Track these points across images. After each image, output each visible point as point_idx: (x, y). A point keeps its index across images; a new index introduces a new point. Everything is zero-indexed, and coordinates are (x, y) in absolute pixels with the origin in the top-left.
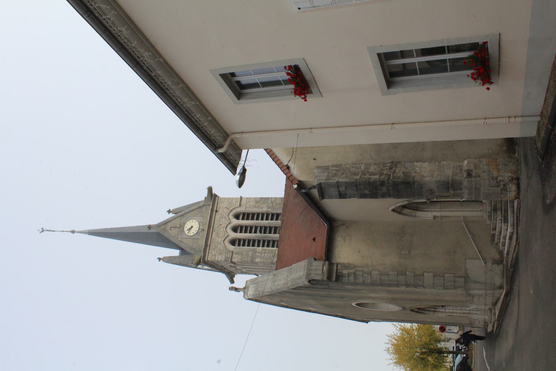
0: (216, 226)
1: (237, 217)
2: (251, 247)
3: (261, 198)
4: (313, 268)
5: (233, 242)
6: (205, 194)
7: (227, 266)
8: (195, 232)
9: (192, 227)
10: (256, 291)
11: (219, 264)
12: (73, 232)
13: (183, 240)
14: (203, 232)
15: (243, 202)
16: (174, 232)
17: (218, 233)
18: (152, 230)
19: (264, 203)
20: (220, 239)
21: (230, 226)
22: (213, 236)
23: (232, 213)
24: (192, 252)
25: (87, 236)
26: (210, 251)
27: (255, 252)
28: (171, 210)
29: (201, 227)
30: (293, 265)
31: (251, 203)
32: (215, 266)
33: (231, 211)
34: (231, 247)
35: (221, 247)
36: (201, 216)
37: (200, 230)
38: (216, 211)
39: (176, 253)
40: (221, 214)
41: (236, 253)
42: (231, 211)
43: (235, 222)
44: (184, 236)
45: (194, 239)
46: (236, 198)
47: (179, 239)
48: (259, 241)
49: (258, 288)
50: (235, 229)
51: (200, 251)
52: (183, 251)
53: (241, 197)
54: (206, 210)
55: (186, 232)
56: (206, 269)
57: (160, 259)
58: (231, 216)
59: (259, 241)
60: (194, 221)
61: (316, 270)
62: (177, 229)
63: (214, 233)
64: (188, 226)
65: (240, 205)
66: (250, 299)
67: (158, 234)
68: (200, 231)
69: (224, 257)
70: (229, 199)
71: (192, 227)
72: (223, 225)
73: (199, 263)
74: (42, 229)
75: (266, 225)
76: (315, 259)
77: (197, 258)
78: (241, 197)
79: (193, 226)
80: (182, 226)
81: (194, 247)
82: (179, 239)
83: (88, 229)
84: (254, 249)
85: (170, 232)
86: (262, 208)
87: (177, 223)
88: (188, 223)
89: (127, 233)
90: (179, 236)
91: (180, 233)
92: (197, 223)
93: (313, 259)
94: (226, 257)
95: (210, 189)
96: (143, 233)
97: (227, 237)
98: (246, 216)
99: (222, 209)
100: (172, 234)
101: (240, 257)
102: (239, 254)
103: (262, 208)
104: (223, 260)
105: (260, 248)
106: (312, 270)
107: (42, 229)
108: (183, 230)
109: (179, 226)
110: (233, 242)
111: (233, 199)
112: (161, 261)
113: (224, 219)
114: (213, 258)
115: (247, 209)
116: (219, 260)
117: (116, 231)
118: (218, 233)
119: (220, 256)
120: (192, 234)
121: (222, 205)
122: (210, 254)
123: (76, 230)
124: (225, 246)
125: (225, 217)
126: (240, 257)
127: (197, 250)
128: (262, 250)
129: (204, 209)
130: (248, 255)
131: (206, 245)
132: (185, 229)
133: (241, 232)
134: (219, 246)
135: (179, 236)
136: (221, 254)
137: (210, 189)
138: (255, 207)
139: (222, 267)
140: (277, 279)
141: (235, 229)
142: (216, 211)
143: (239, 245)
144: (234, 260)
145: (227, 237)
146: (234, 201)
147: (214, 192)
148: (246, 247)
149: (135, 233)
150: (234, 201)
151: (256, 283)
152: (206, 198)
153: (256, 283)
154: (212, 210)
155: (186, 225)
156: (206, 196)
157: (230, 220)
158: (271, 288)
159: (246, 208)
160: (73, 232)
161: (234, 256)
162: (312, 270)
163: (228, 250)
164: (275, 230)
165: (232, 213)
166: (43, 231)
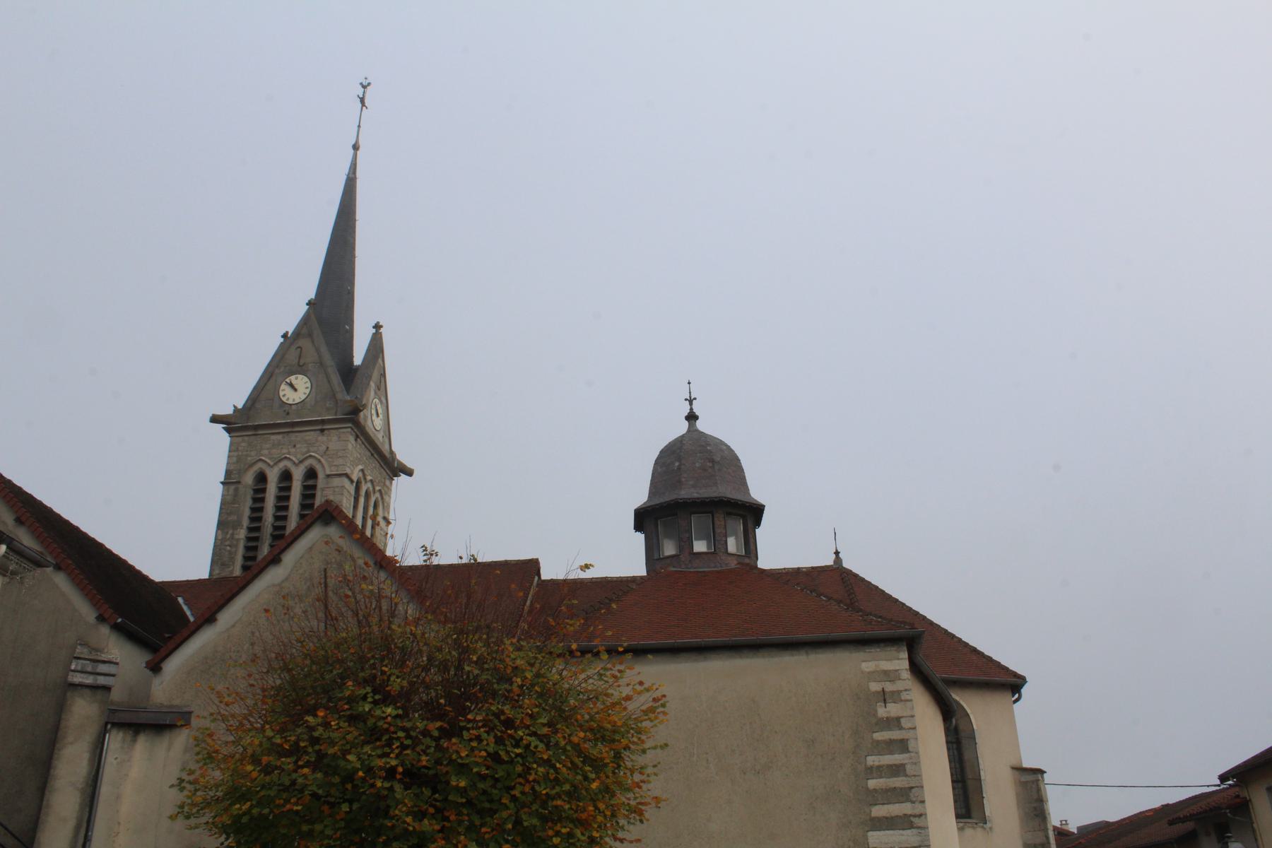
0: (293, 437)
1: (311, 474)
38: (322, 431)
65: (328, 476)
110: (262, 478)
121: (335, 438)
141: (286, 476)
142: (322, 431)
157: (301, 462)
160: (356, 147)
164: (879, 771)
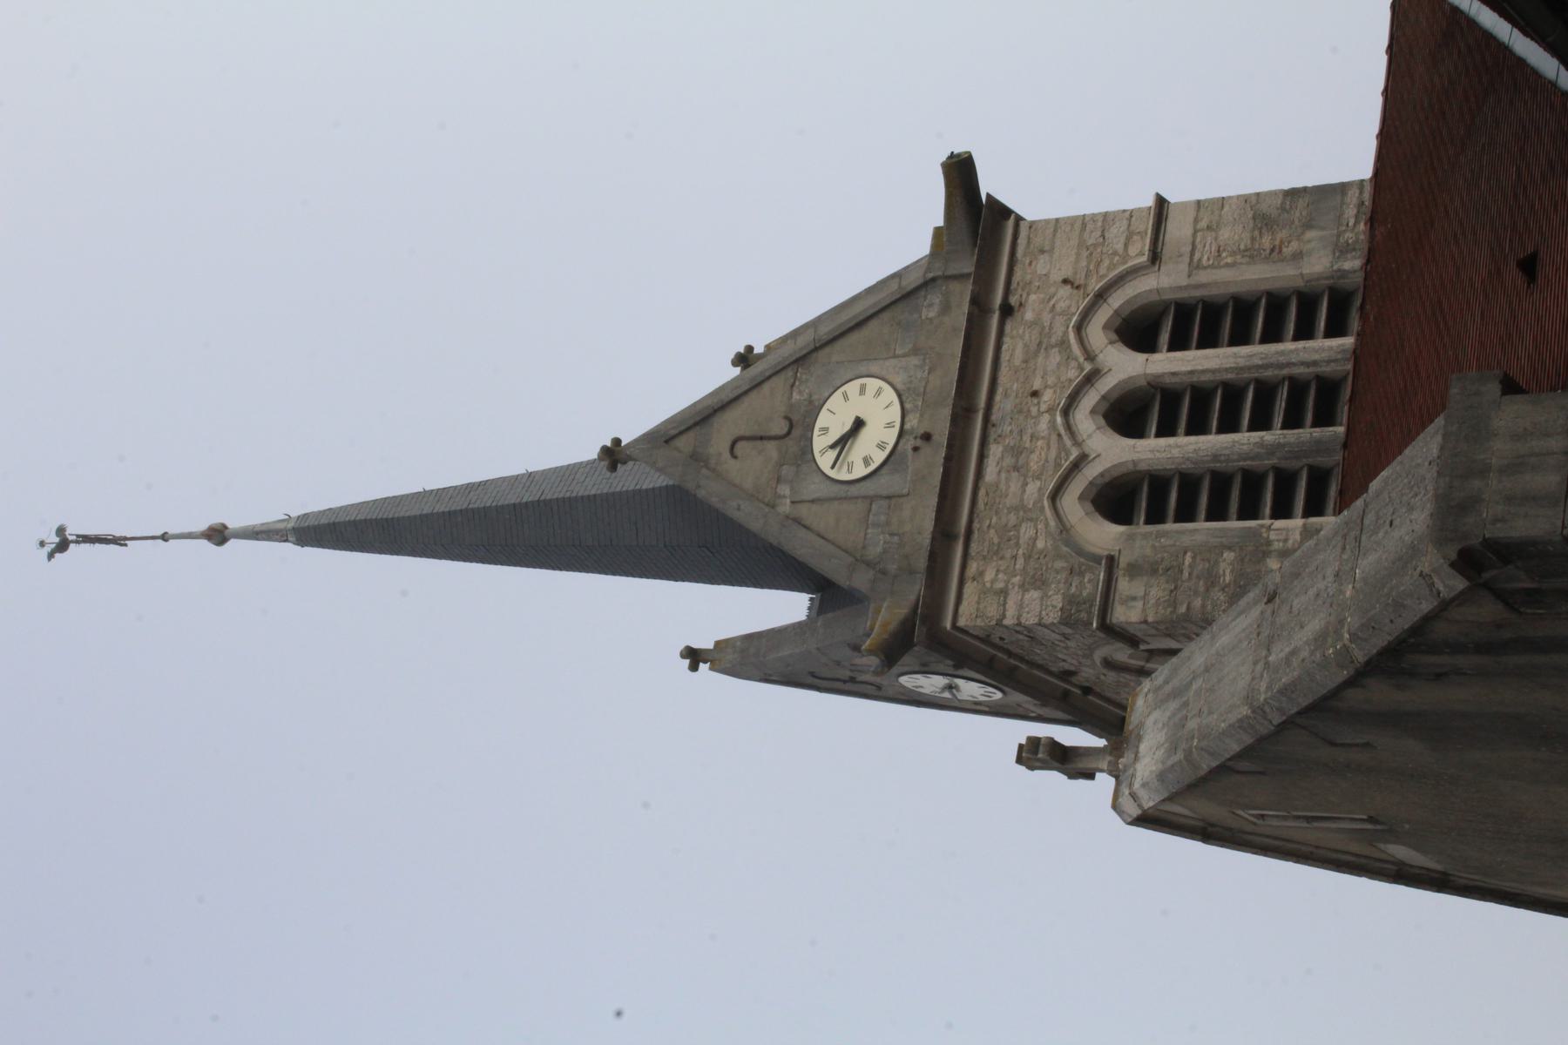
0: (1003, 405)
1: (1138, 332)
2: (1234, 524)
3: (1293, 194)
4: (1499, 450)
5: (1116, 499)
6: (929, 207)
7: (1090, 662)
8: (879, 457)
9: (859, 424)
10: (1173, 749)
11: (1040, 655)
12: (218, 535)
13: (804, 511)
14: (926, 450)
15: (1178, 231)
16: (751, 467)
17: (1017, 451)
18: (630, 478)
19: (1308, 225)
20: (1033, 488)
21: (1090, 399)
22: (990, 473)
23: (1103, 314)
24: (860, 581)
25: (289, 549)
26: (973, 567)
27: (1261, 550)
28: (759, 349)
29: (912, 421)
30: (1375, 485)
31: (1225, 234)
32: (1012, 673)
33: (1101, 296)
34: (1103, 535)
35: (1037, 535)
36: (915, 351)
37: (910, 440)
38: (1007, 311)
39: (786, 607)
40: (1035, 323)
41: (1134, 570)
42: (1101, 296)
43: (1127, 367)
44: (813, 488)
45: (871, 499)
46: (1131, 214)
47: (785, 507)
48: (1285, 482)
49: (1182, 724)
50: (1129, 413)
51: (912, 572)
52: (829, 594)
53: (1161, 202)
54: (946, 308)
55: (825, 461)
56: (975, 708)
57: (694, 657)
58: (1096, 333)
59: (1285, 482)
60: (873, 384)
61: (1516, 466)
62: (771, 447)
63: (995, 450)
64: (832, 420)
65: (1155, 257)
66: (1147, 820)
67: (679, 499)
68: (908, 443)
69: (1058, 601)
70: (1083, 222)
71: (859, 424)
72: (1047, 396)
73: (894, 650)
74: (61, 531)
75: (1326, 369)
76: (1510, 387)
77: (886, 615)
78: (1161, 202)
79: (865, 418)
80: (800, 425)
81: (874, 551)
82: (785, 507)
83: (295, 513)
84: (1255, 533)
85: (732, 467)
86: (1298, 256)
87: (768, 407)
88: (835, 401)
89: (500, 509)
90: (785, 490)
91: (787, 471)
92: (889, 395)
93: (1494, 388)
94: (1071, 601)
95: (960, 172)
96: (591, 499)
97: (1076, 466)
98: (1197, 321)
99: (1044, 293)
100: (739, 480)
101: (1158, 590)
102: (1154, 572)
103: (1298, 256)
104: (1052, 617)
105: (1296, 523)
106: (1484, 471)
107: (61, 531)
108: (806, 453)
109: (779, 427)
110: (1116, 499)
111: (1107, 218)
112: (703, 667)
113: (1056, 357)
114: (992, 611)
115: (1203, 277)
116: (1030, 619)
117: (441, 508)
118: (1017, 451)
119: (1034, 594)
120: (860, 471)
121: (1041, 266)
122: (970, 588)
123: (233, 524)
124: (1064, 528)
125: (1063, 344)
126: (1158, 590)
127: (892, 568)
128: (1307, 533)
129: (930, 306)
130: (1211, 579)
131: (944, 532)
132: (820, 442)
133: (1166, 430)
134: (1026, 532)
135: (785, 490)
136: (1038, 582)
137: (960, 172)
138: (1252, 254)
139: (1066, 675)
140: (1282, 618)
143: (1155, 517)
144: (1124, 614)
145: (1076, 466)
146: (1116, 233)
147: (988, 185)
148: (1202, 529)
149: (548, 503)
150: (1116, 233)
151: (1175, 694)
152: (938, 232)
153: (1175, 694)
154: (979, 305)
155: (823, 419)
156: (940, 221)
157: (1090, 357)
158: (1249, 699)
159: (1195, 266)
160: (218, 535)
161: (1124, 586)
162: (1484, 471)
163: (1080, 552)
165: (1103, 314)
166: (63, 546)
